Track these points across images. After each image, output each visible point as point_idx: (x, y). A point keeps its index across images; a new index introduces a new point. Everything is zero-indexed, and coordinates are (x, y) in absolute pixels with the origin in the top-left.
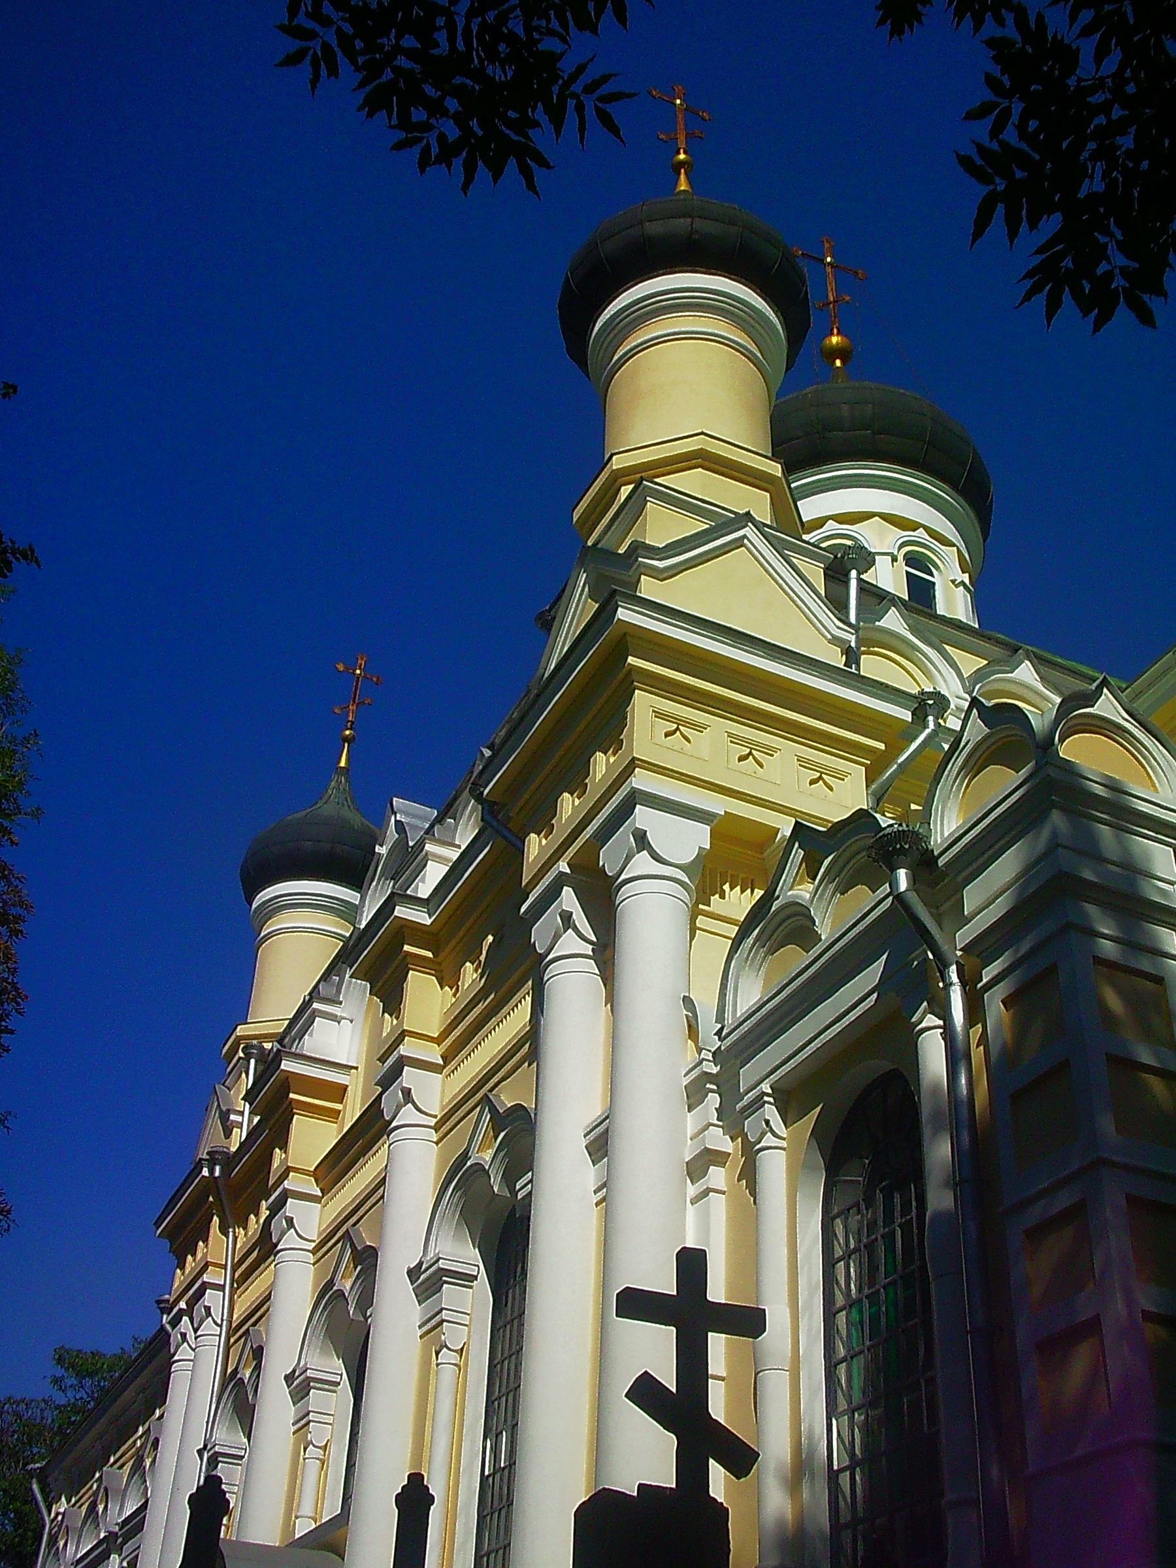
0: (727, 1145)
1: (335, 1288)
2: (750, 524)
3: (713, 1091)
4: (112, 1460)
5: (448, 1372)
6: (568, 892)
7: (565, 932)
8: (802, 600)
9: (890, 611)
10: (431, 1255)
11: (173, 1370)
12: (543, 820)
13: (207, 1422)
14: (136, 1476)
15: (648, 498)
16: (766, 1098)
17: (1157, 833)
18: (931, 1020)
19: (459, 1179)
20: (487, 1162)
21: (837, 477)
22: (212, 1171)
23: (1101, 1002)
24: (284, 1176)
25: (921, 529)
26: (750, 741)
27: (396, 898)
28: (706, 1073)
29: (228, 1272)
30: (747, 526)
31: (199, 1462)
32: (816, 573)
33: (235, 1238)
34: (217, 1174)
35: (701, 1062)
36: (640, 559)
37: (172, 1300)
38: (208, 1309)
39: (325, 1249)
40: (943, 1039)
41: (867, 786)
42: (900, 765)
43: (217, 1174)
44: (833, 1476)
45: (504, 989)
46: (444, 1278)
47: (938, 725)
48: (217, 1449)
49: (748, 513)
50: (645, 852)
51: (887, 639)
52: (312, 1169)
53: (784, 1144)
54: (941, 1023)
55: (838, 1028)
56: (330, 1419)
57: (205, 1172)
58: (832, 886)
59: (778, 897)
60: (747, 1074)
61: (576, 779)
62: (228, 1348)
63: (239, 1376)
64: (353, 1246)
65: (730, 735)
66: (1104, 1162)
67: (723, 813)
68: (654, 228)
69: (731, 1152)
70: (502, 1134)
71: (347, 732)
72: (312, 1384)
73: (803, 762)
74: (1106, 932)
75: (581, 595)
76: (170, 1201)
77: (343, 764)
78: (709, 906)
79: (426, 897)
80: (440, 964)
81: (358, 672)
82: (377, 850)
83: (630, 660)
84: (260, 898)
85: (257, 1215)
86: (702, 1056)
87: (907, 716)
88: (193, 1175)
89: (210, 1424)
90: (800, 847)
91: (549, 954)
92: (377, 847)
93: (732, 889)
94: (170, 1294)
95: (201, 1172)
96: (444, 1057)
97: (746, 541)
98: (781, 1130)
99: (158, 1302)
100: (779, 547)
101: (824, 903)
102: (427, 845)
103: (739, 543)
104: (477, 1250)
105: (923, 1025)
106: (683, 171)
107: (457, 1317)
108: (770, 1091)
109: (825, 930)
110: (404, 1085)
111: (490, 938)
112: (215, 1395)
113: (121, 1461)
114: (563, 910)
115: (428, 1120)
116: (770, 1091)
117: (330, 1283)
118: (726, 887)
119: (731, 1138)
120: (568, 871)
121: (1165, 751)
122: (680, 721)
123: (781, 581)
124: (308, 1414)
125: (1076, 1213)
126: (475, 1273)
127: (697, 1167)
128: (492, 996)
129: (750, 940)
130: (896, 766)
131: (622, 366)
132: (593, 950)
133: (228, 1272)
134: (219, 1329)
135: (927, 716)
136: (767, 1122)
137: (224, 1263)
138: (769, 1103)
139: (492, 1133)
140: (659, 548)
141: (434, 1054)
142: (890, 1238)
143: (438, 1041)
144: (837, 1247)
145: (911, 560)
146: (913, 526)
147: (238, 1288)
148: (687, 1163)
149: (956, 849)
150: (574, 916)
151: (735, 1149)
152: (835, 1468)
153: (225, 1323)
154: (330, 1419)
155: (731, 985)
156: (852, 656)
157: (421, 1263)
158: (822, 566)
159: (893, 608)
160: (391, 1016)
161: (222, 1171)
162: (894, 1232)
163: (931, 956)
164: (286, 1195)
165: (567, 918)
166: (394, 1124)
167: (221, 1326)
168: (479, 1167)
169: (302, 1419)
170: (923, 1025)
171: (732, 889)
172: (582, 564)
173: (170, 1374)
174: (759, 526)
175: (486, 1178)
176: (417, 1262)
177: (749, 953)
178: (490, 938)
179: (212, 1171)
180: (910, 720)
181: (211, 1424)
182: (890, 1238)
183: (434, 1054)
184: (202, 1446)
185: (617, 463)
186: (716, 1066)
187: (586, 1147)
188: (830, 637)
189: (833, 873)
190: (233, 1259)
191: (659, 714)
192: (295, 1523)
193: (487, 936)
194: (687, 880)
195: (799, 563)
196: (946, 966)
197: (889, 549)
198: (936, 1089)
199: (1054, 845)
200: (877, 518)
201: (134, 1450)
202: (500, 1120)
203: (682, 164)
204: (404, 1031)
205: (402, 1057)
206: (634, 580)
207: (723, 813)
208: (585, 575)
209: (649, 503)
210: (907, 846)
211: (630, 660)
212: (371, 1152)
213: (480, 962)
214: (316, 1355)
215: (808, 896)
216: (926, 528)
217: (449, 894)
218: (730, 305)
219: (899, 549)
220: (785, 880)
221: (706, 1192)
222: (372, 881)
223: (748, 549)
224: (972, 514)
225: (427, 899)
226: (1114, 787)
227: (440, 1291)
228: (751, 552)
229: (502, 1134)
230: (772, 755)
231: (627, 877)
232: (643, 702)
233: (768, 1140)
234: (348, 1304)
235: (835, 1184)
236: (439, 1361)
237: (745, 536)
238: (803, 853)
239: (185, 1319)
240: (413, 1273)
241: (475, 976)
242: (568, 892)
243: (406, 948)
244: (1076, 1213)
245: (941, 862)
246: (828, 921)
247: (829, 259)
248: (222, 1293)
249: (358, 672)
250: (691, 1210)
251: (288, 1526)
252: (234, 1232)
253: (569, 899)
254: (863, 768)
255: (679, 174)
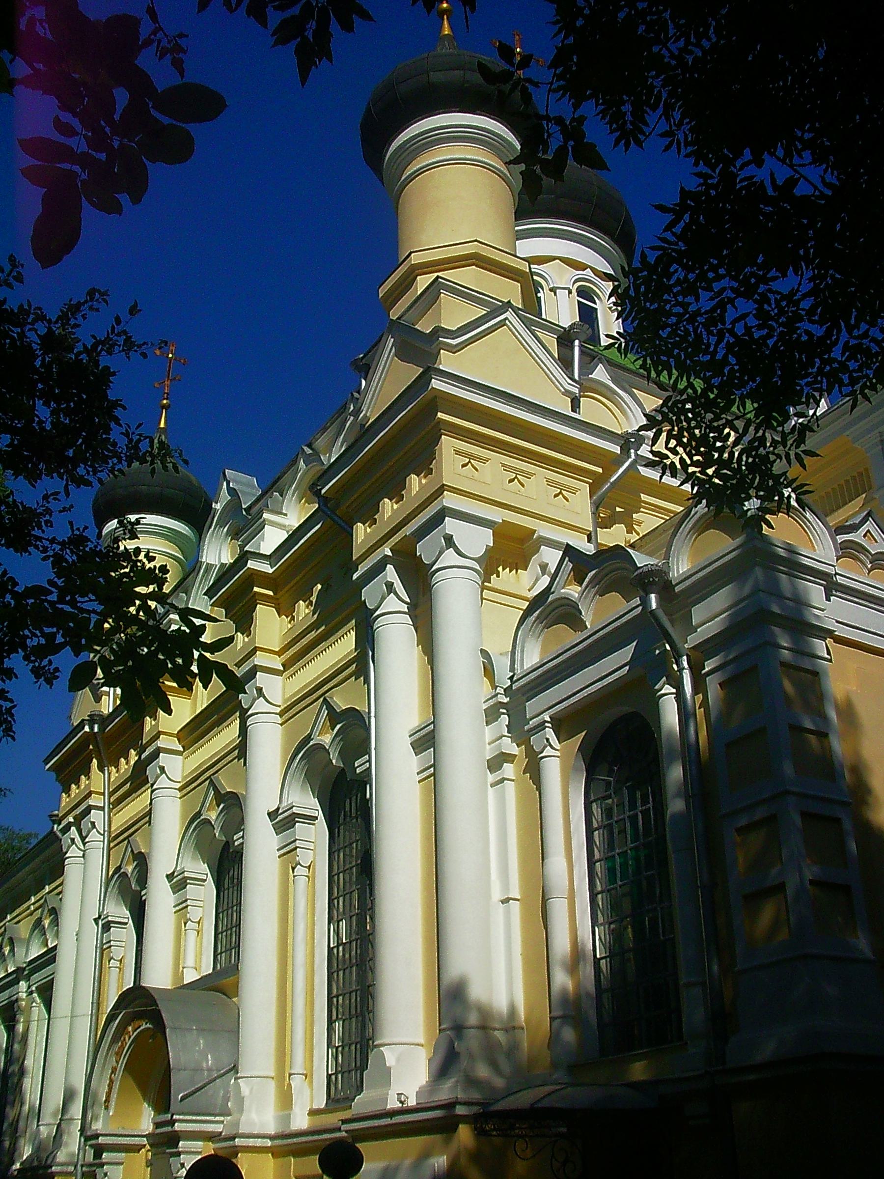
0: (513, 749)
1: (202, 817)
2: (510, 309)
3: (504, 714)
4: (9, 918)
5: (302, 882)
6: (390, 567)
7: (388, 595)
8: (540, 359)
9: (599, 367)
10: (284, 804)
11: (66, 863)
12: (369, 514)
13: (100, 900)
14: (36, 932)
15: (442, 291)
16: (547, 724)
17: (815, 578)
18: (668, 689)
19: (305, 752)
20: (327, 744)
21: (528, 229)
22: (92, 728)
23: (781, 686)
24: (156, 737)
25: (589, 269)
26: (515, 469)
27: (249, 555)
28: (500, 702)
29: (106, 797)
30: (508, 310)
31: (96, 927)
32: (552, 342)
33: (109, 774)
34: (96, 730)
35: (496, 695)
36: (440, 339)
37: (60, 815)
38: (93, 823)
39: (189, 789)
40: (676, 701)
41: (590, 497)
42: (612, 484)
43: (96, 730)
44: (597, 961)
45: (333, 623)
46: (297, 819)
47: (637, 455)
48: (110, 918)
49: (509, 302)
50: (451, 549)
51: (594, 386)
52: (176, 732)
53: (558, 754)
54: (674, 691)
55: (599, 685)
56: (201, 904)
57: (87, 729)
58: (594, 590)
59: (553, 593)
60: (532, 707)
61: (396, 491)
62: (109, 850)
63: (122, 871)
64: (216, 789)
65: (503, 465)
66: (788, 792)
67: (501, 521)
68: (437, 77)
69: (517, 754)
70: (338, 726)
71: (165, 402)
72: (188, 881)
73: (550, 483)
74: (785, 645)
75: (389, 354)
76: (57, 747)
77: (162, 425)
78: (490, 583)
79: (269, 554)
80: (278, 599)
81: (170, 356)
82: (213, 506)
83: (440, 415)
84: (108, 527)
85: (126, 758)
86: (498, 691)
87: (617, 450)
88: (77, 730)
89: (102, 902)
90: (569, 561)
91: (377, 609)
92: (214, 505)
93: (504, 569)
94: (58, 810)
95: (83, 728)
96: (283, 665)
97: (507, 322)
98: (557, 745)
99: (51, 816)
100: (528, 324)
101: (588, 601)
102: (264, 514)
103: (502, 324)
104: (316, 799)
105: (663, 692)
106: (445, 17)
107: (306, 845)
108: (549, 720)
109: (588, 618)
110: (258, 685)
111: (319, 586)
112: (103, 884)
113: (17, 919)
114: (387, 581)
115: (272, 708)
116: (549, 720)
117: (199, 814)
118: (500, 569)
119: (517, 745)
120: (390, 554)
121: (820, 523)
122: (471, 456)
123: (521, 339)
124: (186, 901)
125: (771, 820)
126: (316, 815)
127: (496, 763)
128: (323, 627)
129: (532, 618)
130: (609, 484)
131: (410, 181)
132: (408, 608)
133: (106, 797)
134: (102, 837)
135: (630, 449)
136: (548, 740)
137: (102, 791)
138: (549, 727)
139: (328, 724)
140: (453, 331)
141: (276, 663)
142: (633, 819)
143: (279, 653)
144: (594, 822)
145: (582, 292)
146: (582, 267)
147: (113, 808)
148: (488, 761)
149: (688, 583)
150: (395, 584)
151: (521, 751)
152: (598, 956)
153: (106, 833)
154: (201, 904)
155: (518, 648)
156: (575, 405)
157: (278, 809)
158: (556, 337)
159: (600, 365)
160: (243, 634)
161: (99, 728)
162: (637, 815)
163: (668, 647)
164: (89, 809)
165: (390, 586)
166: (250, 712)
167: (103, 835)
168: (320, 747)
169: (181, 903)
170: (663, 692)
171: (504, 569)
172: (390, 331)
173: (64, 867)
174: (515, 310)
175: (326, 754)
176: (276, 807)
177: (532, 626)
178: (319, 586)
179: (92, 728)
180: (619, 452)
181: (103, 902)
182: (633, 819)
183: (276, 663)
184: (97, 916)
185: (415, 259)
186: (506, 697)
187: (411, 744)
188: (563, 390)
189: (593, 584)
190: (109, 789)
191: (457, 452)
192: (183, 971)
193: (316, 585)
194: (478, 568)
195: (543, 337)
196: (681, 656)
197: (566, 285)
198: (671, 733)
199: (755, 591)
200: (558, 261)
201: (28, 911)
202: (334, 717)
203: (445, 11)
204: (256, 647)
205: (255, 666)
206: (435, 352)
207: (501, 521)
208: (392, 340)
209: (442, 295)
210: (657, 580)
211: (440, 415)
212: (225, 724)
213: (312, 602)
214: (190, 859)
215: (577, 595)
216: (592, 269)
217: (287, 554)
218: (494, 140)
219: (574, 283)
220: (558, 582)
221: (502, 780)
222: (210, 527)
223: (508, 327)
224: (622, 256)
225: (270, 555)
226: (791, 550)
227: (293, 827)
228: (511, 330)
229: (338, 726)
230: (530, 478)
231: (440, 566)
232: (448, 444)
233: (548, 751)
234: (214, 829)
235: (592, 779)
236: (295, 874)
237: (506, 319)
238: (571, 565)
239: (73, 828)
240: (272, 815)
241: (307, 611)
242: (390, 567)
243: (256, 589)
244: (771, 820)
245: (677, 589)
246: (591, 613)
247: (518, 50)
248: (102, 812)
249: (170, 356)
250: (491, 790)
251: (178, 973)
252: (108, 770)
253: (391, 573)
254: (588, 485)
255: (443, 19)
